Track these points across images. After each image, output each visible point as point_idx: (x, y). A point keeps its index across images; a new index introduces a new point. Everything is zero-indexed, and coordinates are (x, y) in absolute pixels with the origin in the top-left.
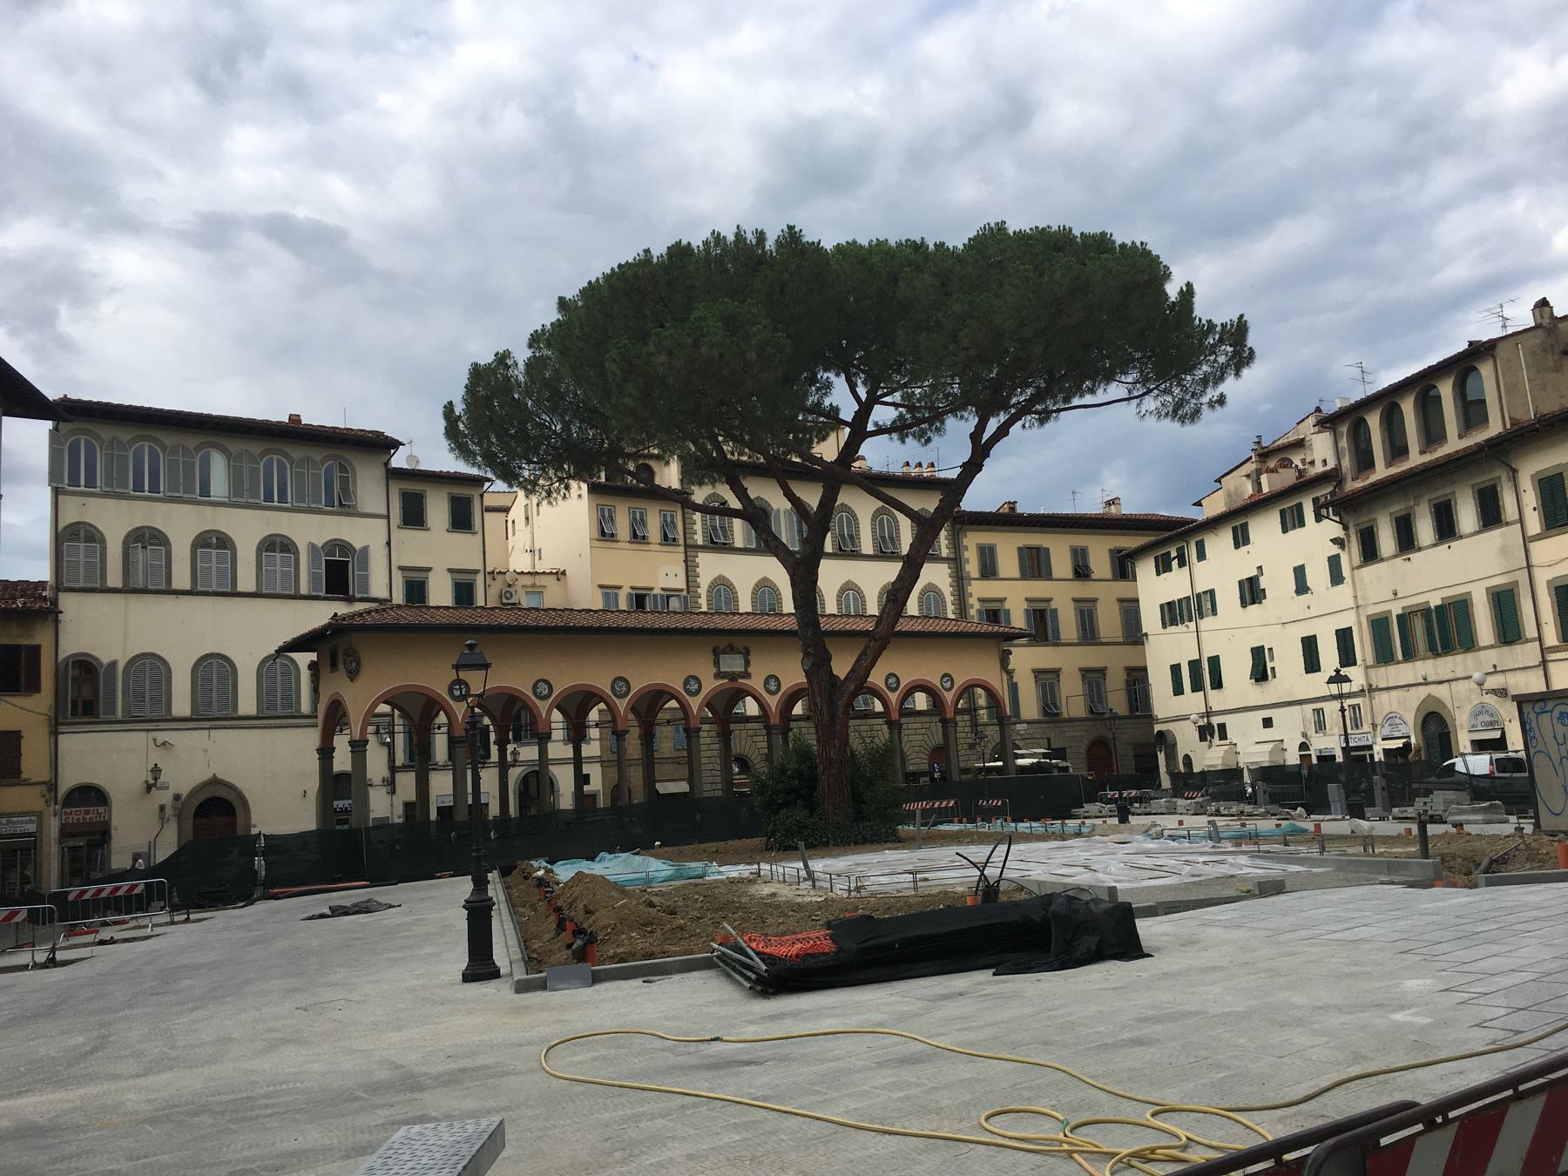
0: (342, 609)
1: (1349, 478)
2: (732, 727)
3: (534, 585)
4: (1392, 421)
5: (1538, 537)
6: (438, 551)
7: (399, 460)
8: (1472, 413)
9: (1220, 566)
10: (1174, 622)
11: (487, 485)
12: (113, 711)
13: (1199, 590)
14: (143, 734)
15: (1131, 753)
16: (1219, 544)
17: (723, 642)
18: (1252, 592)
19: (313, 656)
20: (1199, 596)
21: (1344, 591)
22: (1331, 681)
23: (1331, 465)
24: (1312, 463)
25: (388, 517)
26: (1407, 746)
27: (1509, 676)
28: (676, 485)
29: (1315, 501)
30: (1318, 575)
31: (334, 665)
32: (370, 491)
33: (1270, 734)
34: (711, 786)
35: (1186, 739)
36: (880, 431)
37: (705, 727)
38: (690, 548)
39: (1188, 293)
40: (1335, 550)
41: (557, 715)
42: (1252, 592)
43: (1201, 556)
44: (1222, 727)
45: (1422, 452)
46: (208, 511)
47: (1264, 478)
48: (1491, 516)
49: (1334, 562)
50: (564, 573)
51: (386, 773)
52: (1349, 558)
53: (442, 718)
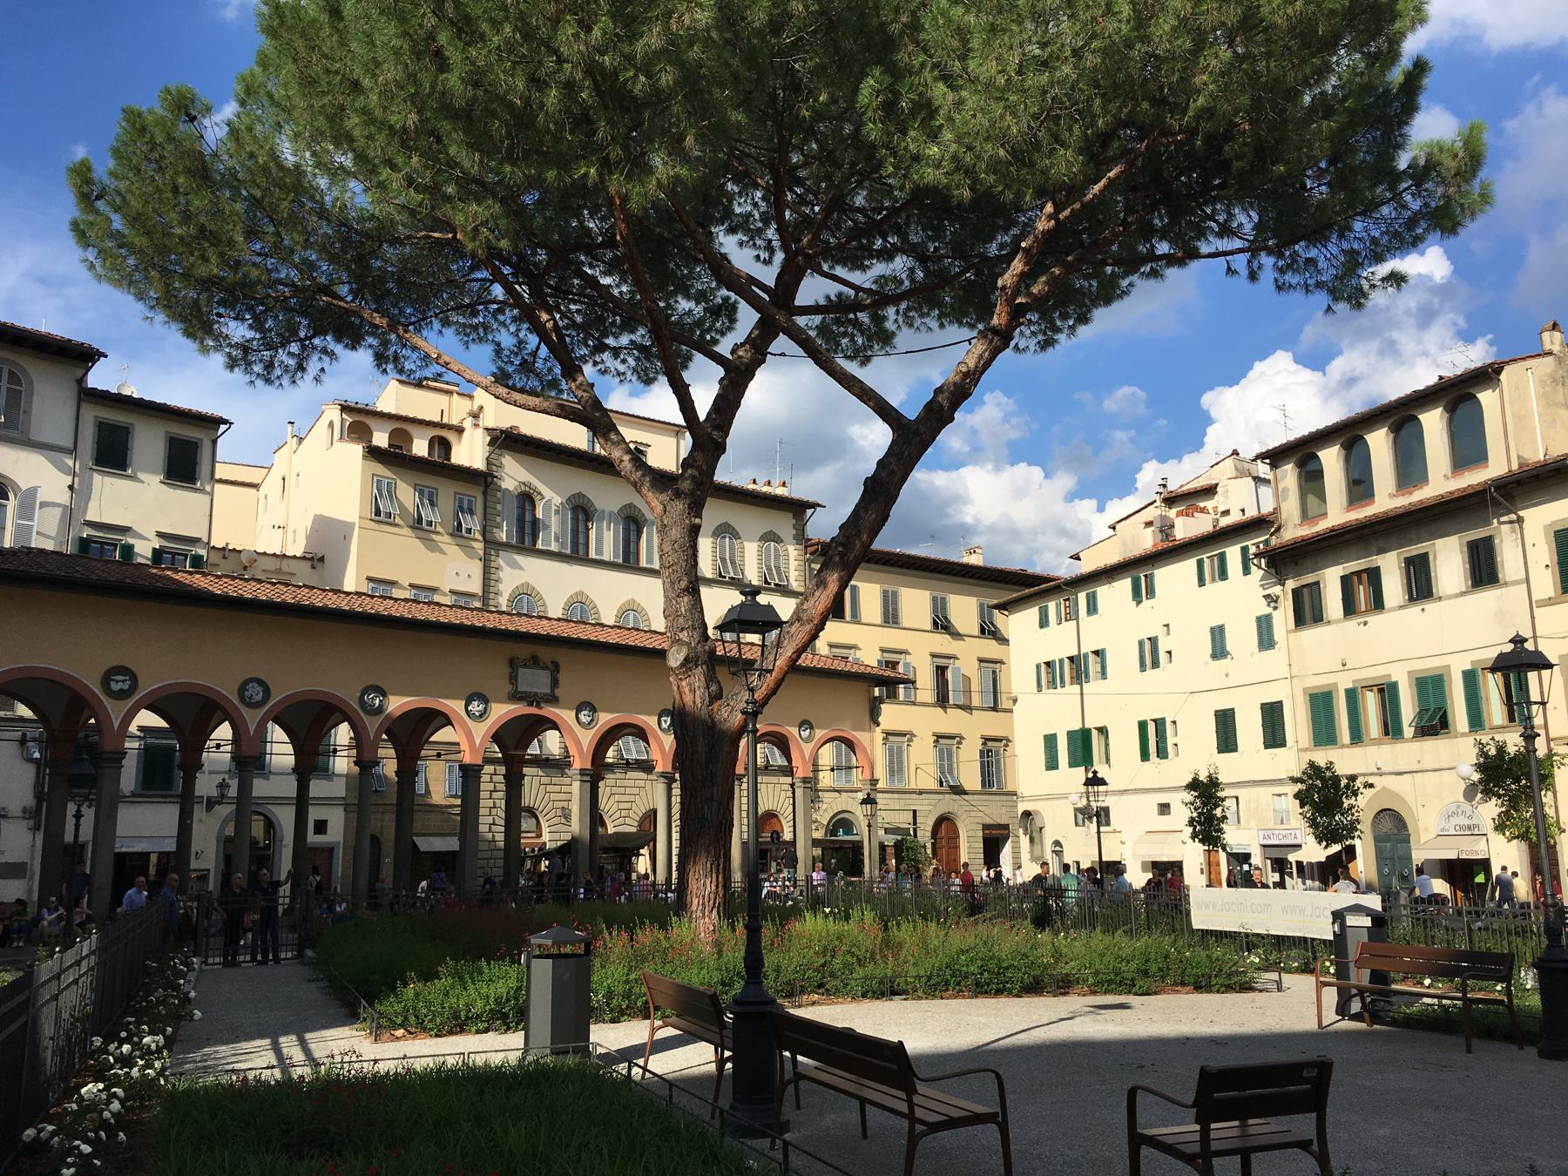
1: (1290, 524)
2: (526, 770)
3: (279, 571)
5: (1549, 602)
7: (100, 378)
8: (1468, 448)
10: (1052, 684)
11: (223, 427)
13: (1087, 648)
15: (980, 834)
17: (523, 651)
18: (1150, 654)
20: (1086, 656)
21: (1274, 660)
24: (1226, 513)
28: (479, 464)
29: (1244, 550)
30: (1242, 638)
32: (50, 404)
34: (458, 802)
35: (1058, 822)
37: (489, 769)
38: (491, 544)
41: (277, 733)
43: (1092, 608)
45: (1392, 496)
48: (1483, 570)
49: (1264, 624)
50: (322, 559)
52: (1283, 617)
53: (224, 731)
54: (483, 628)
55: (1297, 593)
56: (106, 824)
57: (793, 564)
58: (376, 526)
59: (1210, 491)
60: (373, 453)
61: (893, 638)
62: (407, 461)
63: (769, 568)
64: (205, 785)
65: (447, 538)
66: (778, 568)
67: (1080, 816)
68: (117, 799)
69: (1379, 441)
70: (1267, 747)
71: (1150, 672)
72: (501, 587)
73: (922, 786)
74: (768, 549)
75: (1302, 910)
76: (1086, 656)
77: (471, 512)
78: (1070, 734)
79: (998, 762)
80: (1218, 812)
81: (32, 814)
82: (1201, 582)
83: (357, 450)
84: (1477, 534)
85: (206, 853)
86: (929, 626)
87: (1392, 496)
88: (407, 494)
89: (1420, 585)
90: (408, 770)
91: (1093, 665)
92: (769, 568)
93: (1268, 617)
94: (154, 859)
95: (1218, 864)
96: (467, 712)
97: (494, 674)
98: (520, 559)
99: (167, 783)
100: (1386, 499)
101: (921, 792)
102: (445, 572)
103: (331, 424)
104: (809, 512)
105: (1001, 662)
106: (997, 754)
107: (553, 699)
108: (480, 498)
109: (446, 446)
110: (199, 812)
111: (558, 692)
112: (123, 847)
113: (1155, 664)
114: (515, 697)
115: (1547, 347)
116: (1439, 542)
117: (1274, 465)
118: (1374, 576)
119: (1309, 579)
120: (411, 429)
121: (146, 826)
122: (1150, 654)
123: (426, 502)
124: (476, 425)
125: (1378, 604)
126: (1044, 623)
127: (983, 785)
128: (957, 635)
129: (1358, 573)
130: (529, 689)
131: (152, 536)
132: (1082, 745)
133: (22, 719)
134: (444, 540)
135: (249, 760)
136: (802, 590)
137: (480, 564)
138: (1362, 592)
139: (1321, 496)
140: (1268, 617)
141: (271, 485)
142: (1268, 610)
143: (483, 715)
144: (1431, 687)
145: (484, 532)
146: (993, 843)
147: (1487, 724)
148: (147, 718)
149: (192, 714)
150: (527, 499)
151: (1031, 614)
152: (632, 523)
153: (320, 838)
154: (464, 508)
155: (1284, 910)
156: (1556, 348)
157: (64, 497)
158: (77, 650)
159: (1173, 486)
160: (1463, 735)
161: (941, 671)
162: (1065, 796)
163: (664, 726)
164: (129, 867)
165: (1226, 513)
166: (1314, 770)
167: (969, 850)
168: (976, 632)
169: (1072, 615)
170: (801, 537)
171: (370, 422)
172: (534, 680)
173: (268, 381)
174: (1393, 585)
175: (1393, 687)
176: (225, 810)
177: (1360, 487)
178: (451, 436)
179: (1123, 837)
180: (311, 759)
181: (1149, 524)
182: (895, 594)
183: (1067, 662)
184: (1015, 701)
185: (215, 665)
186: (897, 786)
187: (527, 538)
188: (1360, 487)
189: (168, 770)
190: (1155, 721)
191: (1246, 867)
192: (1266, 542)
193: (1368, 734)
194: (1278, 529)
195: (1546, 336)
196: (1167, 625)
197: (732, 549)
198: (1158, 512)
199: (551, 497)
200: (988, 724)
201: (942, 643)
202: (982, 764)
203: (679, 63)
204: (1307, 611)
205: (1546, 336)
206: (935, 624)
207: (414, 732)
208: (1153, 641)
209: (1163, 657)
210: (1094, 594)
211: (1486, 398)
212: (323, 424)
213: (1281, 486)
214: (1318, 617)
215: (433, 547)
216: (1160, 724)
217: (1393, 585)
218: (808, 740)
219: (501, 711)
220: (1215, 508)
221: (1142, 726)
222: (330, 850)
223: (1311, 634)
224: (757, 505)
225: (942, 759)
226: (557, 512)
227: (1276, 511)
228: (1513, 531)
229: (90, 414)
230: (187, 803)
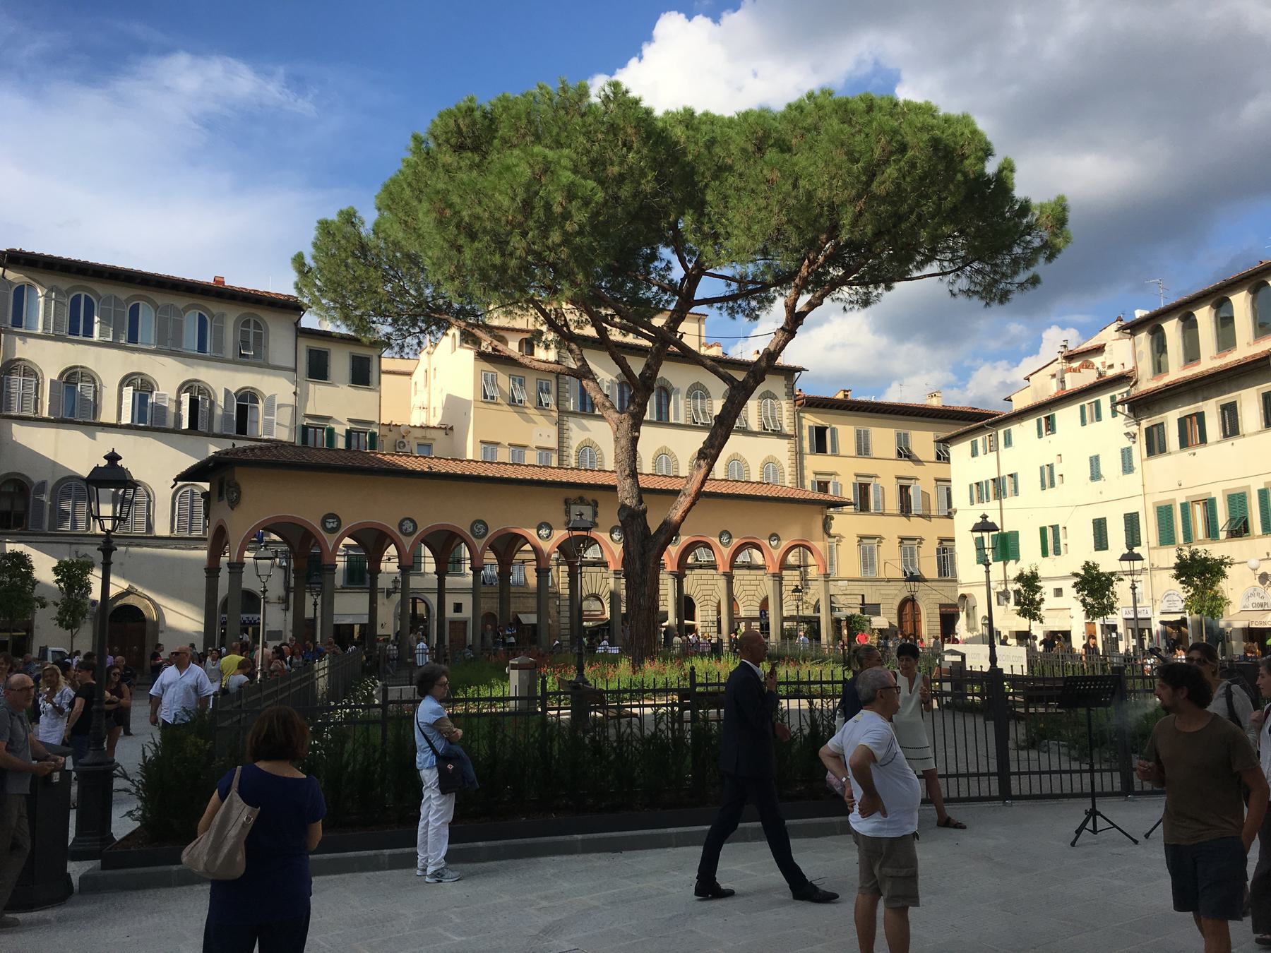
0: (241, 444)
4: (1190, 325)
6: (337, 403)
9: (1024, 448)
12: (40, 525)
13: (1004, 473)
14: (66, 547)
18: (1048, 478)
19: (206, 486)
22: (1124, 558)
23: (1128, 367)
24: (1111, 366)
25: (295, 370)
29: (1113, 398)
30: (1112, 465)
31: (221, 494)
32: (280, 344)
36: (708, 302)
38: (563, 412)
39: (1008, 167)
40: (1127, 443)
41: (426, 551)
42: (1048, 478)
43: (1008, 442)
45: (1212, 358)
46: (136, 356)
47: (1068, 377)
49: (1126, 454)
50: (451, 429)
51: (282, 592)
53: (392, 550)
55: (1149, 431)
56: (328, 605)
59: (1100, 350)
60: (481, 356)
61: (865, 466)
63: (766, 418)
64: (383, 582)
65: (533, 411)
66: (773, 418)
67: (1001, 598)
68: (334, 590)
69: (1204, 315)
70: (1096, 550)
71: (1048, 490)
73: (889, 576)
74: (766, 405)
77: (548, 392)
80: (1037, 597)
81: (284, 601)
82: (1083, 423)
85: (387, 623)
86: (894, 455)
87: (1212, 358)
88: (504, 381)
89: (1231, 427)
90: (505, 573)
92: (766, 418)
94: (357, 628)
97: (554, 511)
98: (585, 422)
99: (362, 581)
100: (1210, 361)
101: (889, 581)
103: (454, 335)
104: (797, 374)
108: (554, 382)
110: (381, 598)
112: (338, 620)
113: (1052, 485)
118: (1200, 417)
119: (1156, 419)
121: (350, 608)
126: (974, 453)
127: (940, 575)
128: (918, 462)
129: (1190, 416)
131: (345, 421)
133: (275, 542)
135: (409, 566)
137: (556, 428)
141: (418, 376)
144: (1237, 501)
148: (348, 541)
149: (373, 541)
153: (458, 615)
154: (543, 390)
157: (291, 400)
158: (306, 503)
159: (1072, 347)
161: (904, 490)
164: (342, 634)
165: (1111, 366)
166: (1088, 567)
167: (929, 627)
168: (934, 458)
169: (994, 448)
170: (791, 394)
173: (402, 357)
176: (397, 597)
180: (446, 564)
181: (1054, 376)
182: (866, 432)
183: (991, 483)
185: (382, 509)
186: (869, 576)
188: (1226, 338)
189: (362, 575)
191: (1114, 635)
192: (1127, 392)
193: (1196, 535)
194: (1136, 383)
201: (906, 468)
204: (1155, 445)
206: (899, 454)
207: (507, 545)
208: (1051, 466)
214: (1163, 450)
215: (528, 420)
216: (1055, 528)
218: (776, 548)
219: (560, 534)
220: (1103, 363)
221: (1043, 531)
222: (464, 623)
223: (1159, 462)
225: (905, 556)
229: (304, 344)
230: (373, 592)
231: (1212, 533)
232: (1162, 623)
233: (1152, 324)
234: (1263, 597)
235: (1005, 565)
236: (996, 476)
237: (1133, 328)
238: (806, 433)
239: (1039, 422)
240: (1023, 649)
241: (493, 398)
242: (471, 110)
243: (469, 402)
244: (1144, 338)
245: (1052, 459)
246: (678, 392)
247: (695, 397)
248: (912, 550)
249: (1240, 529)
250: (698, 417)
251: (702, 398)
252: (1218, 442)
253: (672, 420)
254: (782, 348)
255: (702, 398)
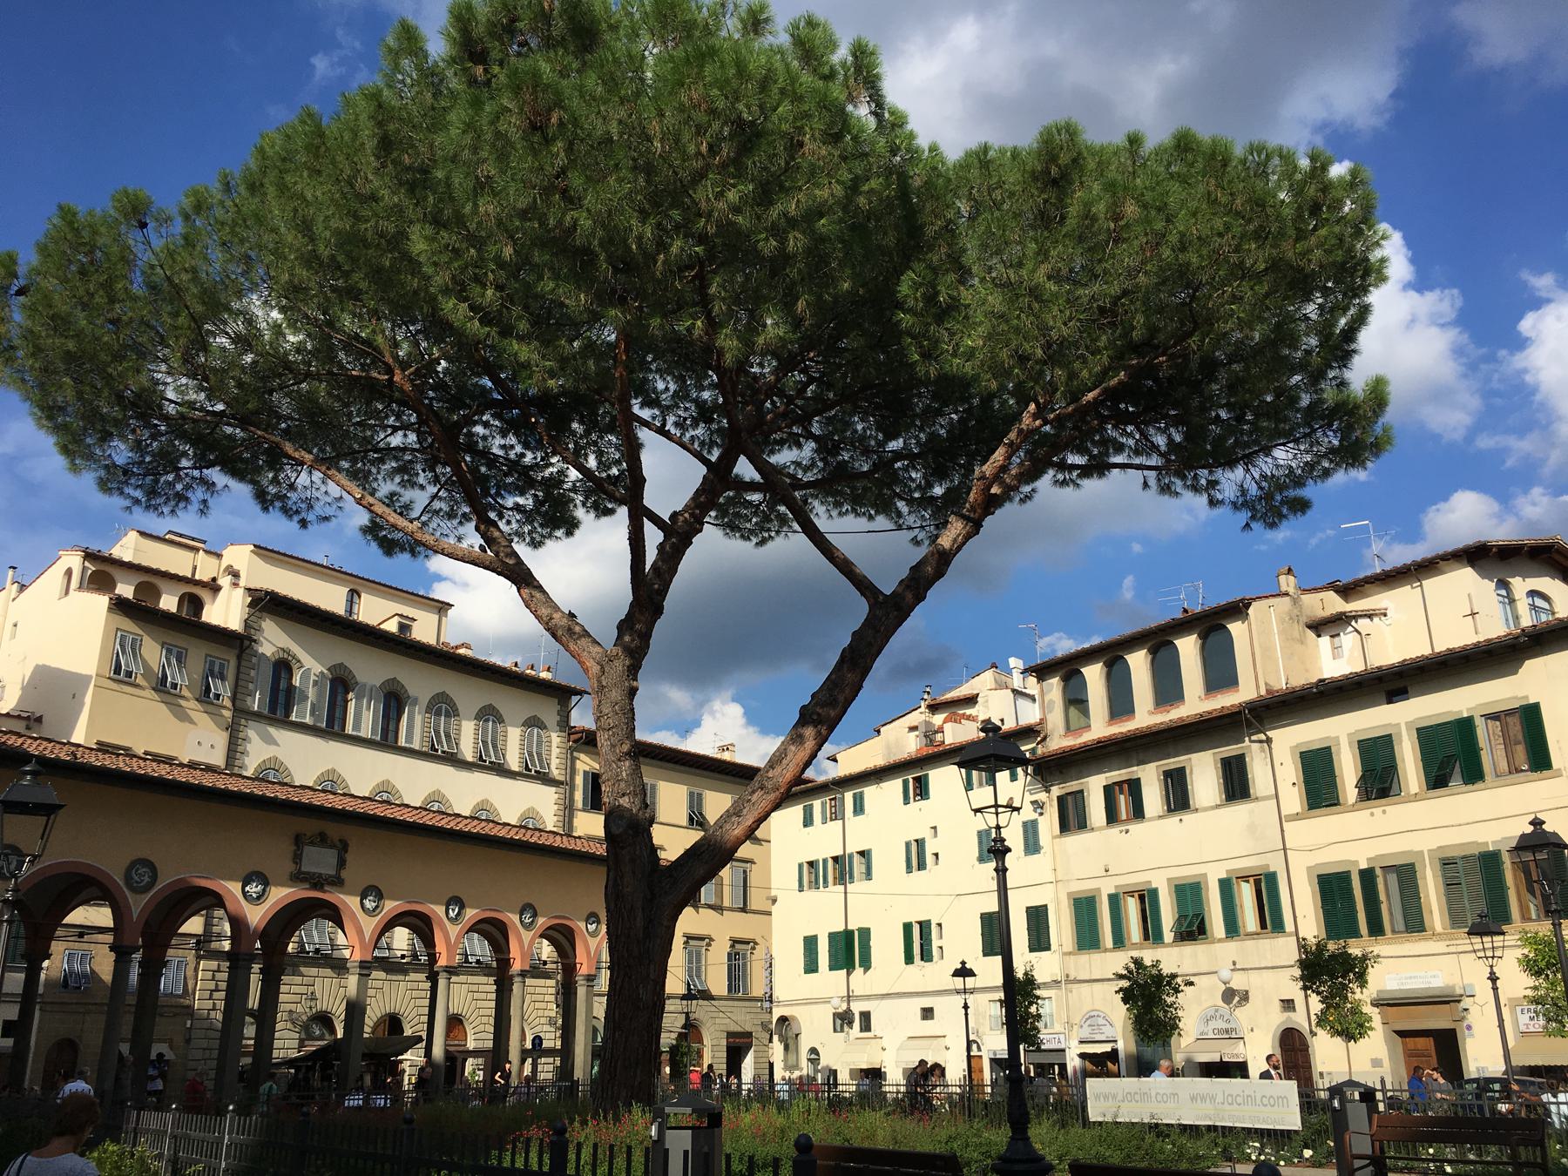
1: (1056, 735)
5: (1296, 817)
8: (1220, 673)
15: (724, 1042)
16: (885, 795)
17: (311, 826)
18: (917, 856)
20: (851, 856)
22: (957, 973)
26: (1115, 1052)
27: (1253, 975)
33: (928, 1027)
35: (815, 1029)
43: (859, 808)
44: (866, 1017)
48: (1236, 784)
50: (39, 720)
52: (1049, 823)
54: (263, 796)
55: (1061, 800)
57: (555, 751)
58: (114, 686)
60: (120, 605)
62: (156, 615)
63: (531, 754)
67: (839, 1022)
69: (1138, 662)
70: (1032, 950)
71: (916, 873)
72: (247, 760)
74: (531, 735)
75: (1213, 1098)
76: (851, 856)
77: (223, 679)
78: (832, 936)
79: (745, 965)
83: (102, 601)
84: (1230, 750)
86: (685, 822)
88: (153, 652)
89: (1178, 797)
91: (858, 866)
92: (531, 754)
93: (1034, 823)
95: (981, 1071)
96: (244, 893)
97: (277, 855)
98: (272, 730)
100: (1146, 715)
102: (192, 741)
103: (69, 572)
104: (575, 699)
105: (752, 862)
106: (744, 957)
107: (337, 882)
108: (233, 663)
109: (195, 604)
111: (344, 874)
113: (922, 866)
114: (297, 878)
115: (1284, 588)
116: (1195, 757)
117: (1041, 679)
118: (1134, 787)
119: (1073, 786)
120: (161, 584)
122: (917, 856)
123: (174, 661)
124: (236, 585)
125: (1138, 813)
126: (808, 821)
127: (730, 990)
129: (1120, 784)
130: (313, 870)
132: (849, 950)
134: (191, 705)
136: (562, 778)
138: (1123, 801)
139: (1085, 712)
140: (1034, 823)
142: (1034, 816)
143: (260, 897)
144: (1189, 893)
145: (234, 699)
146: (736, 1050)
147: (1241, 931)
150: (283, 666)
151: (794, 813)
152: (394, 702)
155: (1193, 1099)
156: (1291, 590)
160: (1220, 940)
162: (826, 1001)
163: (452, 914)
170: (564, 724)
171: (115, 572)
172: (320, 860)
174: (1153, 796)
175: (1154, 893)
177: (1121, 703)
178: (204, 594)
179: (884, 1043)
181: (913, 729)
183: (830, 862)
184: (774, 901)
187: (280, 709)
188: (1121, 703)
190: (920, 923)
194: (1044, 739)
195: (1283, 578)
196: (935, 828)
197: (495, 732)
198: (923, 717)
199: (311, 666)
200: (740, 925)
202: (730, 967)
203: (810, 231)
204: (1072, 817)
205: (1283, 578)
206: (691, 819)
208: (920, 843)
209: (929, 859)
210: (861, 795)
211: (1236, 628)
212: (57, 572)
213: (1047, 699)
214: (1082, 825)
215: (182, 716)
216: (925, 926)
217: (1153, 796)
221: (907, 928)
223: (1075, 840)
224: (525, 688)
225: (690, 962)
226: (315, 683)
227: (1042, 721)
228: (1263, 750)
231: (1152, 933)
232: (1083, 1056)
233: (1067, 668)
234: (1228, 1021)
235: (848, 974)
236: (839, 852)
237: (1041, 672)
238: (579, 780)
239: (905, 783)
240: (1293, 1084)
241: (129, 674)
242: (317, 142)
243: (83, 680)
244: (1055, 682)
245: (925, 833)
246: (415, 702)
247: (438, 714)
248: (699, 955)
249: (1192, 930)
250: (439, 742)
251: (448, 715)
252: (1218, 807)
253: (402, 742)
254: (959, 548)
255: (448, 715)
